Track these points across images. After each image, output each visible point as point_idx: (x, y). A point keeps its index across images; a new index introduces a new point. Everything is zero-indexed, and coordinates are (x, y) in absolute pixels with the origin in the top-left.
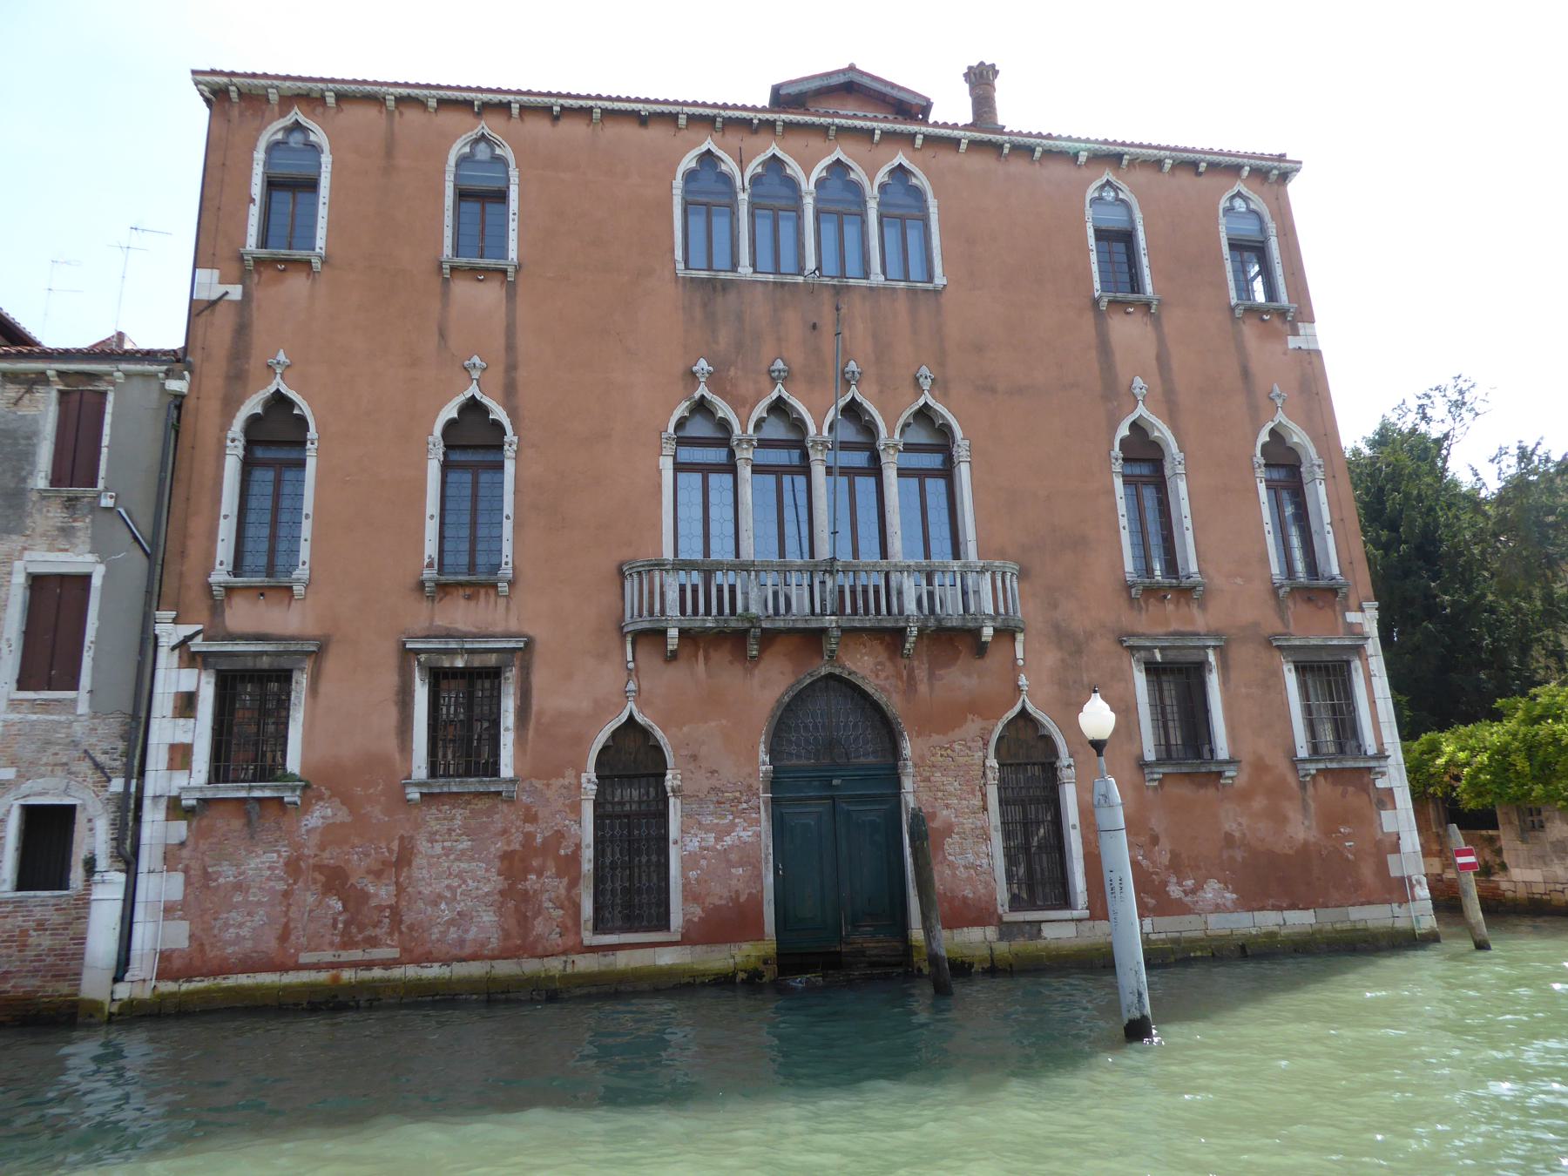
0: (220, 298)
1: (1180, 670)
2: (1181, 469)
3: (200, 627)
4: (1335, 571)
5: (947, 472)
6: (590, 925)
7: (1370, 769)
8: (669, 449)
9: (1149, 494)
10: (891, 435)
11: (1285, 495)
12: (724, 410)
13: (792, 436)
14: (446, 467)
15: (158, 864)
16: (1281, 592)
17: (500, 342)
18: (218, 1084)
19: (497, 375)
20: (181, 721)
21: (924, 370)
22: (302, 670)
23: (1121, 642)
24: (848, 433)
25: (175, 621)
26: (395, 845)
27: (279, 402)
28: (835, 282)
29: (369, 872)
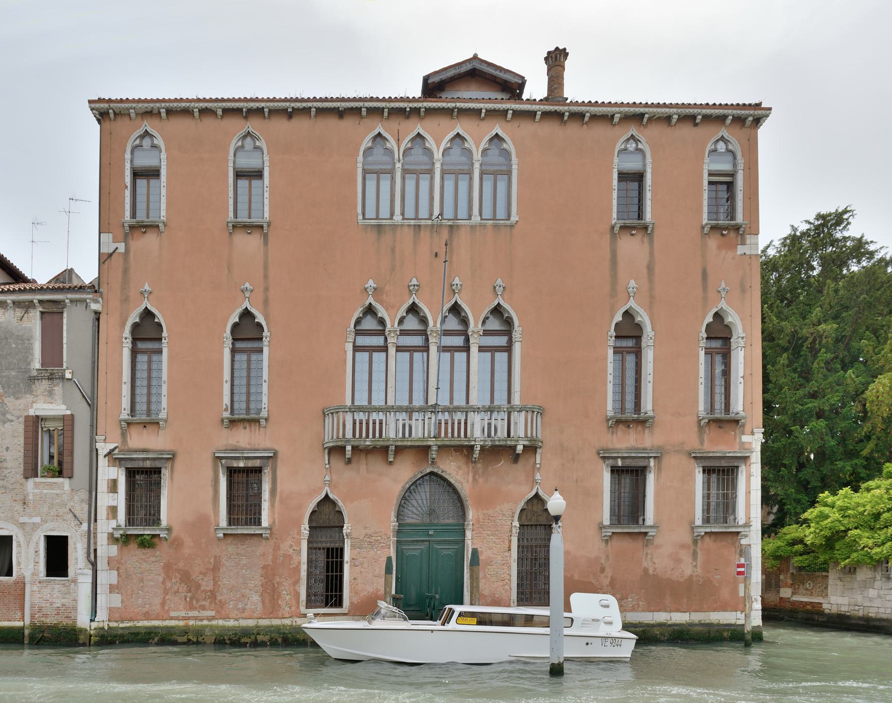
0: (114, 252)
1: (632, 471)
2: (651, 343)
6: (304, 603)
7: (738, 533)
9: (630, 359)
12: (382, 312)
14: (234, 351)
15: (106, 567)
16: (702, 423)
20: (111, 494)
21: (499, 281)
22: (166, 468)
26: (212, 560)
27: (147, 314)
28: (450, 223)
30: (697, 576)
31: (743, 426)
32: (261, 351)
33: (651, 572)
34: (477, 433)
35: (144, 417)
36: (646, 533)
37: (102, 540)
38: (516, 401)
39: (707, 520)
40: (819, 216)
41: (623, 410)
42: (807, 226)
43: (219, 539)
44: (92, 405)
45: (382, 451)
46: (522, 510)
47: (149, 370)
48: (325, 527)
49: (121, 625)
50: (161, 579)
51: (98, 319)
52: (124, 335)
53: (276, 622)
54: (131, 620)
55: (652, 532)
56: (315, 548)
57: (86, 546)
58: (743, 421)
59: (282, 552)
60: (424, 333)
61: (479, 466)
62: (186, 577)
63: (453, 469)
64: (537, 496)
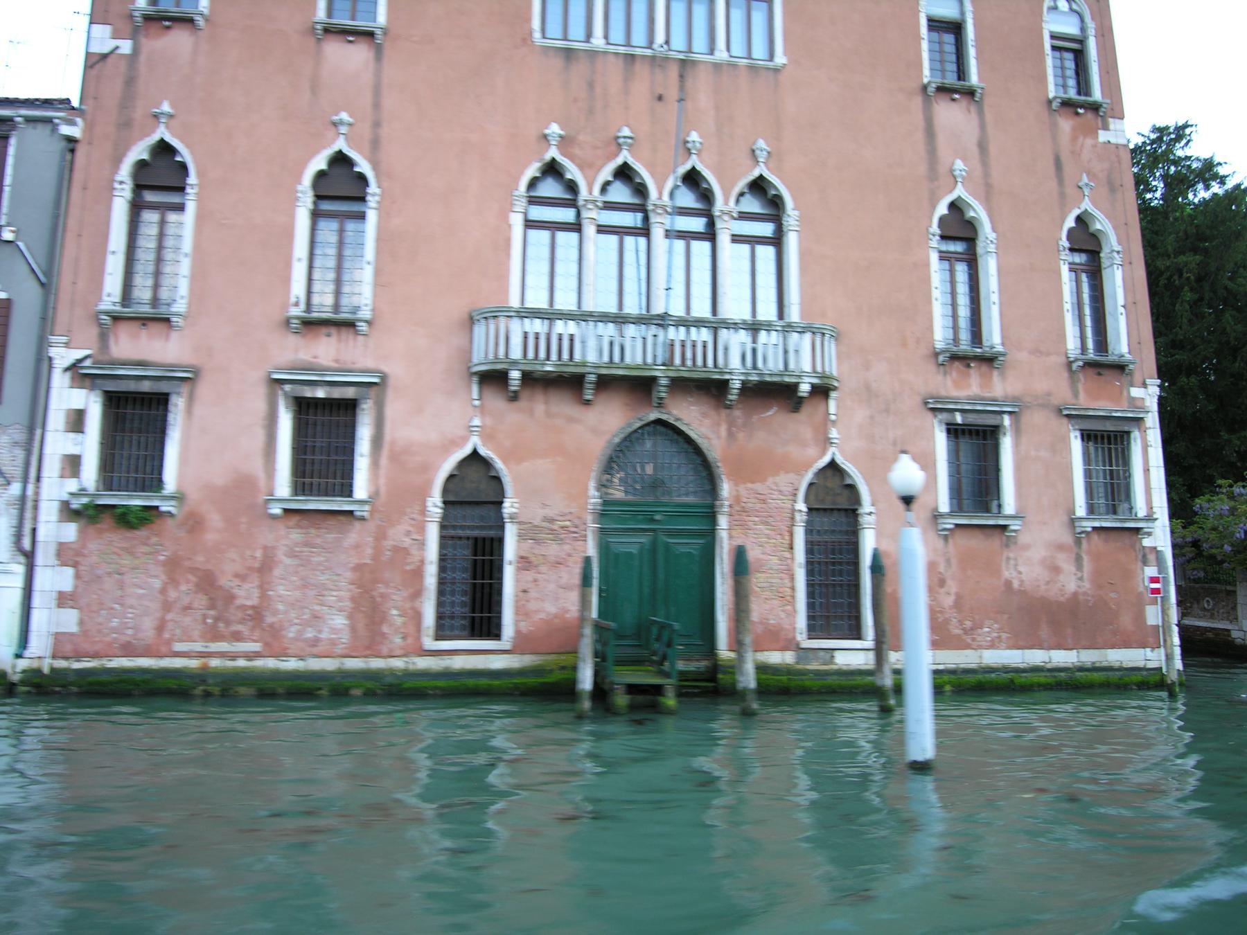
0: (112, 52)
1: (977, 432)
2: (992, 248)
3: (88, 352)
4: (1124, 349)
5: (777, 241)
6: (431, 632)
7: (1138, 530)
8: (520, 205)
9: (961, 270)
10: (726, 202)
11: (1084, 277)
12: (573, 171)
13: (636, 201)
14: (316, 215)
15: (52, 560)
16: (1074, 366)
17: (367, 99)
18: (945, 848)
19: (366, 130)
20: (72, 435)
21: (761, 143)
22: (178, 394)
23: (926, 403)
24: (687, 199)
25: (67, 345)
26: (259, 554)
27: (164, 149)
28: (681, 56)
29: (237, 576)
30: (1085, 593)
31: (1131, 374)
32: (361, 217)
33: (1016, 584)
34: (735, 363)
35: (146, 309)
36: (1004, 527)
37: (49, 513)
38: (794, 315)
39: (1091, 509)
40: (1156, 129)
41: (956, 340)
42: (1140, 140)
43: (274, 517)
44: (47, 286)
45: (569, 383)
46: (811, 485)
47: (161, 236)
48: (469, 503)
49: (77, 665)
50: (157, 584)
51: (72, 151)
52: (118, 178)
53: (377, 664)
54: (95, 656)
55: (1015, 525)
56: (452, 538)
57: (15, 522)
58: (1131, 367)
59: (388, 543)
60: (642, 209)
61: (737, 413)
62: (207, 582)
63: (692, 417)
64: (833, 465)
